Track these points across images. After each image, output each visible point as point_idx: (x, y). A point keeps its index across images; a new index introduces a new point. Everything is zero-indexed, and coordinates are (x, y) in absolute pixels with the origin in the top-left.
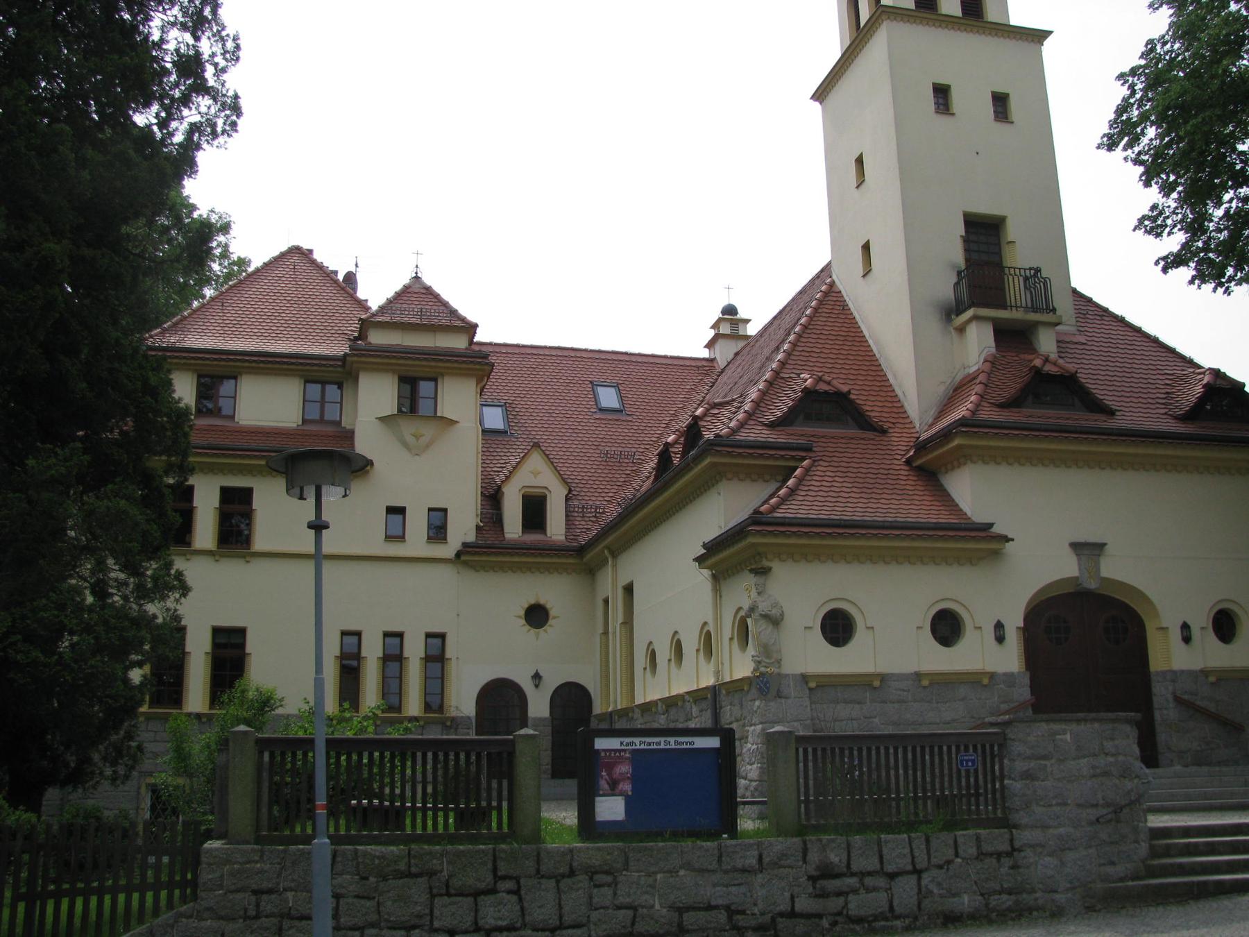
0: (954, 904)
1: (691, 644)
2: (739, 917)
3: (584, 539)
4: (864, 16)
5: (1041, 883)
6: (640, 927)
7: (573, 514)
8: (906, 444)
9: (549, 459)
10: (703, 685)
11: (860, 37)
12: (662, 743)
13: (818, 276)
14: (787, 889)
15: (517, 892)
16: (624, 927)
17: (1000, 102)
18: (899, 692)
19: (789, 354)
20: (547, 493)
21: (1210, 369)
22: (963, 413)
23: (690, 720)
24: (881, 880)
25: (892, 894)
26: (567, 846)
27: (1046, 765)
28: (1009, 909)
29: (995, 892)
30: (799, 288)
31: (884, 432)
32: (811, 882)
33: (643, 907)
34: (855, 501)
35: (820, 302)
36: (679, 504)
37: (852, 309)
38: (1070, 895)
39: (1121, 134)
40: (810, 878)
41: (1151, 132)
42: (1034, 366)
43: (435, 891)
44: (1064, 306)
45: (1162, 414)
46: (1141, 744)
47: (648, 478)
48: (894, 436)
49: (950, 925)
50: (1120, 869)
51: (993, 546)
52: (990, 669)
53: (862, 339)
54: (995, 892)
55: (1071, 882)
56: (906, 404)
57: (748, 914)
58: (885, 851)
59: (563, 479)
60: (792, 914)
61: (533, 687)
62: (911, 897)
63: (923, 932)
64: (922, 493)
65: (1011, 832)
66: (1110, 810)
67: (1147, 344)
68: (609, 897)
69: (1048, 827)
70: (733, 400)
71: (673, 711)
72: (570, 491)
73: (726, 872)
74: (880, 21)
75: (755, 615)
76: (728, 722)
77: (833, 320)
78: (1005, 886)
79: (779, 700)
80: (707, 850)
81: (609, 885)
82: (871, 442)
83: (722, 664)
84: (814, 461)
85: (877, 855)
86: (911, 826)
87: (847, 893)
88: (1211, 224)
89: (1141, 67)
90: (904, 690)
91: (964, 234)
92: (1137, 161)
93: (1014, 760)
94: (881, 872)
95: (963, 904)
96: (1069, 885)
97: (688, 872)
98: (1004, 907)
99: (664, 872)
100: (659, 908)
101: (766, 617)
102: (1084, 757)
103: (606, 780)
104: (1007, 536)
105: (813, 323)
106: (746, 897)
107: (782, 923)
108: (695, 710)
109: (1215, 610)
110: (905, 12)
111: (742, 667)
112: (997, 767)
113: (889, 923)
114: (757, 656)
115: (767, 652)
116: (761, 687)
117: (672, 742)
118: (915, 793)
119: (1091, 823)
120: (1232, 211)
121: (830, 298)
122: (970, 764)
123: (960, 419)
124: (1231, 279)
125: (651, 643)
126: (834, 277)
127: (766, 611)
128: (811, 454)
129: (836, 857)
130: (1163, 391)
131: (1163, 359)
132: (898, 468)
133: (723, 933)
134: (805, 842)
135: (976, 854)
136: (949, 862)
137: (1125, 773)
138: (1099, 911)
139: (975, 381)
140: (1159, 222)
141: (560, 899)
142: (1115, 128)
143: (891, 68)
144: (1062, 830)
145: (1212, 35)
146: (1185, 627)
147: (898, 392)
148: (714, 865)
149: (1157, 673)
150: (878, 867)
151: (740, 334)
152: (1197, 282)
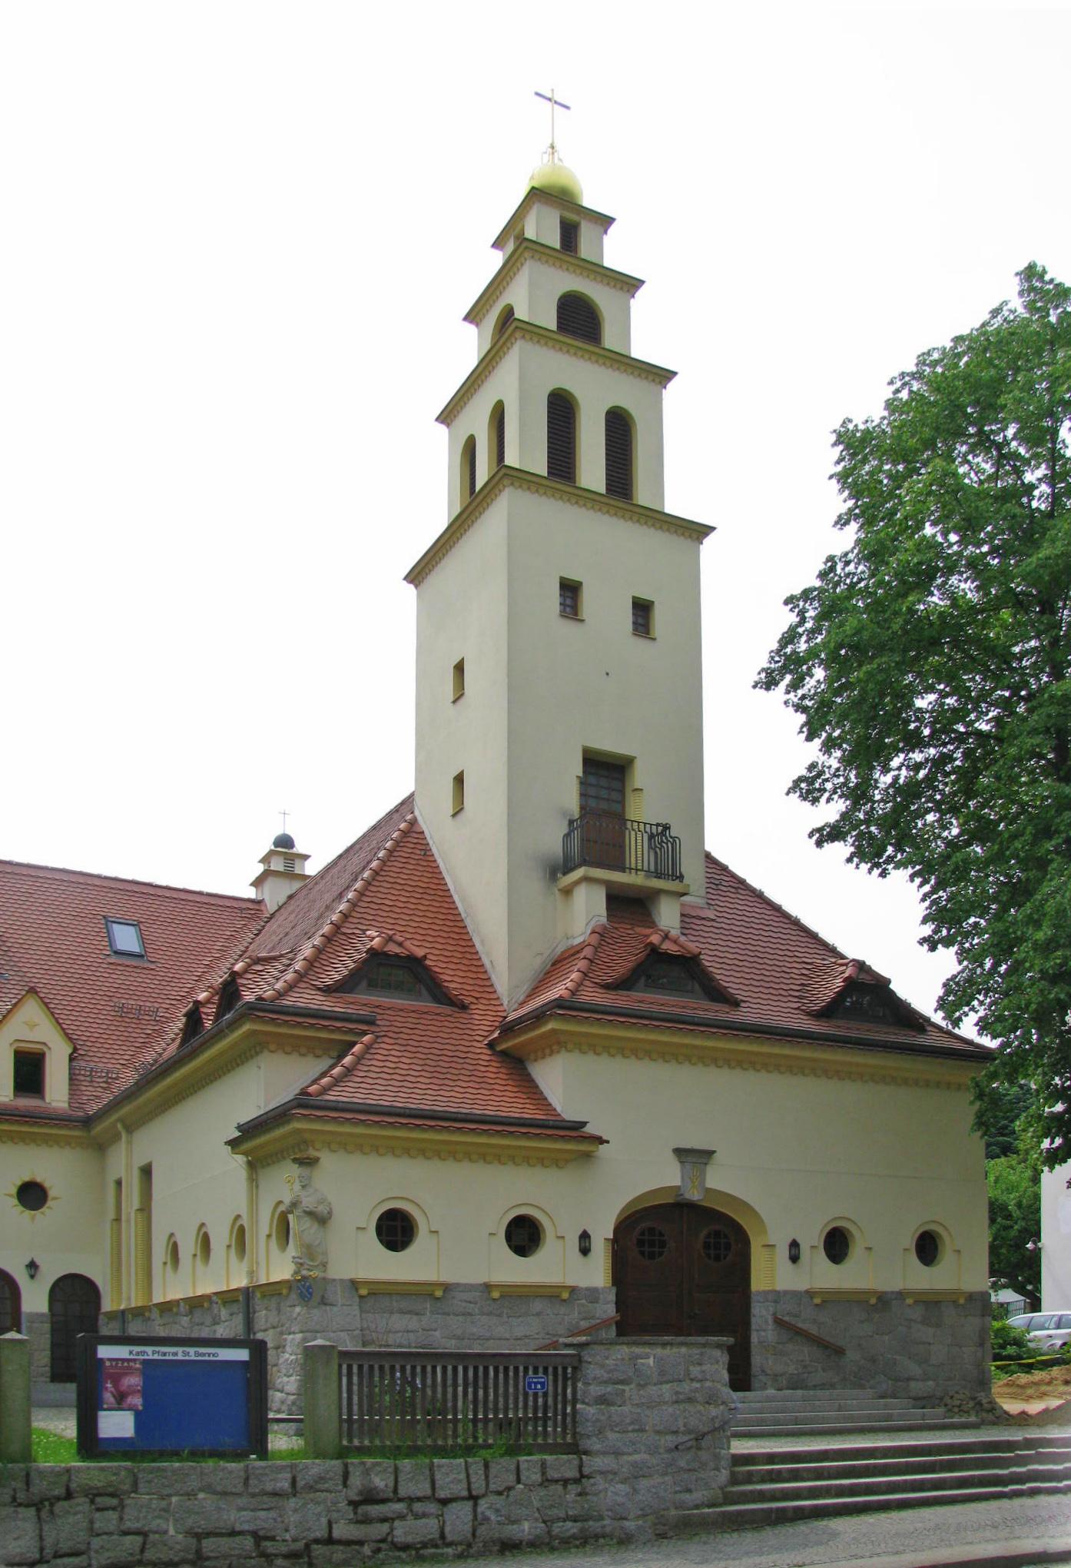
0: (512, 1531)
1: (220, 1238)
2: (268, 1544)
3: (93, 1108)
4: (482, 478)
5: (611, 1510)
6: (150, 1555)
7: (78, 1077)
8: (490, 1023)
9: (48, 1008)
10: (234, 1286)
11: (475, 504)
13: (397, 810)
14: (324, 1513)
16: (131, 1554)
17: (642, 610)
18: (464, 1304)
19: (354, 904)
20: (45, 1049)
21: (854, 960)
22: (561, 992)
23: (218, 1324)
24: (432, 1505)
25: (444, 1522)
26: (63, 1465)
27: (624, 1391)
28: (574, 1537)
29: (559, 1519)
30: (372, 821)
31: (464, 1007)
32: (351, 1508)
33: (156, 1532)
34: (424, 1086)
35: (397, 843)
36: (240, 1056)
37: (437, 856)
38: (640, 1522)
39: (784, 670)
40: (351, 1503)
41: (819, 673)
42: (651, 943)
44: (693, 873)
45: (795, 1009)
46: (732, 1369)
47: (173, 1040)
48: (478, 1011)
49: (507, 1553)
50: (698, 1496)
51: (584, 1147)
52: (570, 1282)
53: (446, 894)
54: (559, 1519)
55: (642, 1510)
56: (493, 978)
57: (278, 1541)
58: (438, 1476)
59: (67, 1034)
60: (330, 1541)
61: (27, 1277)
62: (466, 1524)
63: (477, 1560)
64: (504, 1083)
65: (581, 1459)
66: (692, 1436)
67: (786, 926)
68: (114, 1522)
69: (623, 1454)
70: (282, 956)
71: (198, 1313)
72: (75, 1050)
73: (253, 1495)
74: (501, 487)
75: (298, 1212)
76: (262, 1328)
77: (411, 867)
78: (570, 1513)
79: (324, 1307)
80: (231, 1472)
81: (114, 1509)
82: (449, 1019)
83: (258, 1263)
84: (377, 1037)
85: (429, 1480)
86: (468, 1451)
87: (393, 1519)
88: (876, 792)
89: (815, 589)
90: (470, 1302)
91: (581, 774)
92: (799, 708)
93: (589, 1384)
94: (433, 1498)
95: (523, 1531)
96: (640, 1513)
97: (208, 1496)
98: (568, 1534)
99: (182, 1495)
100: (174, 1534)
101: (310, 1214)
102: (667, 1382)
103: (112, 1392)
104: (601, 1138)
105: (386, 868)
106: (276, 1522)
107: (318, 1550)
108: (224, 1313)
109: (834, 1225)
110: (529, 478)
111: (280, 1268)
112: (569, 1391)
113: (439, 1551)
114: (298, 1257)
115: (310, 1253)
116: (302, 1292)
117: (192, 1353)
118: (475, 1414)
119: (669, 1451)
120: (901, 781)
121: (409, 839)
122: (539, 1386)
123: (556, 999)
124: (890, 860)
125: (172, 1235)
126: (417, 813)
127: (311, 1208)
128: (373, 1028)
129: (381, 1482)
130: (798, 982)
131: (802, 945)
132: (479, 1051)
133: (248, 1560)
134: (346, 1466)
135: (540, 1480)
136: (509, 1489)
137: (711, 1399)
138: (671, 1538)
139: (577, 956)
140: (817, 786)
141: (41, 1530)
142: (778, 662)
143: (509, 552)
144: (637, 1457)
145: (902, 561)
146: (794, 1245)
147: (486, 961)
148: (240, 1488)
149: (759, 1293)
150: (429, 1492)
151: (296, 872)
152: (856, 860)
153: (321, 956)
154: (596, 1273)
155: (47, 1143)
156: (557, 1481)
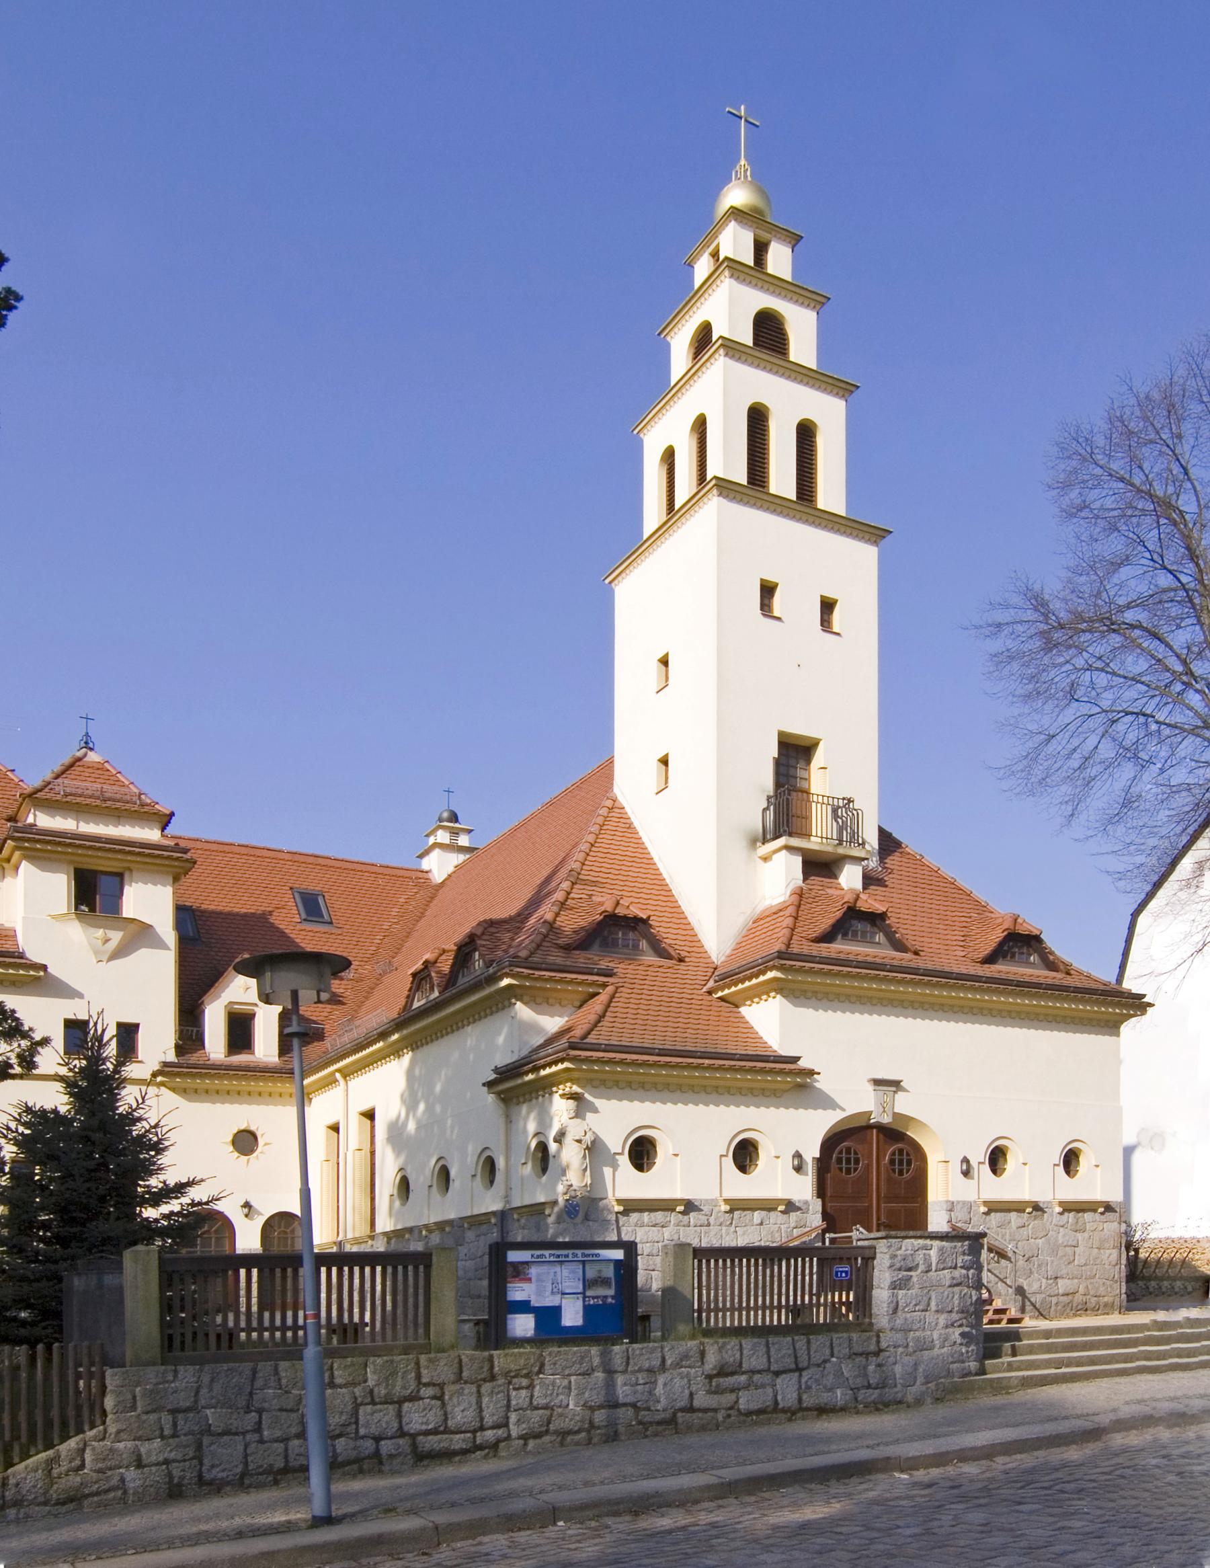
12: (571, 1256)
15: (440, 1398)
33: (560, 1407)
43: (359, 1400)
122: (844, 1275)
154: (803, 1188)
156: (861, 1354)
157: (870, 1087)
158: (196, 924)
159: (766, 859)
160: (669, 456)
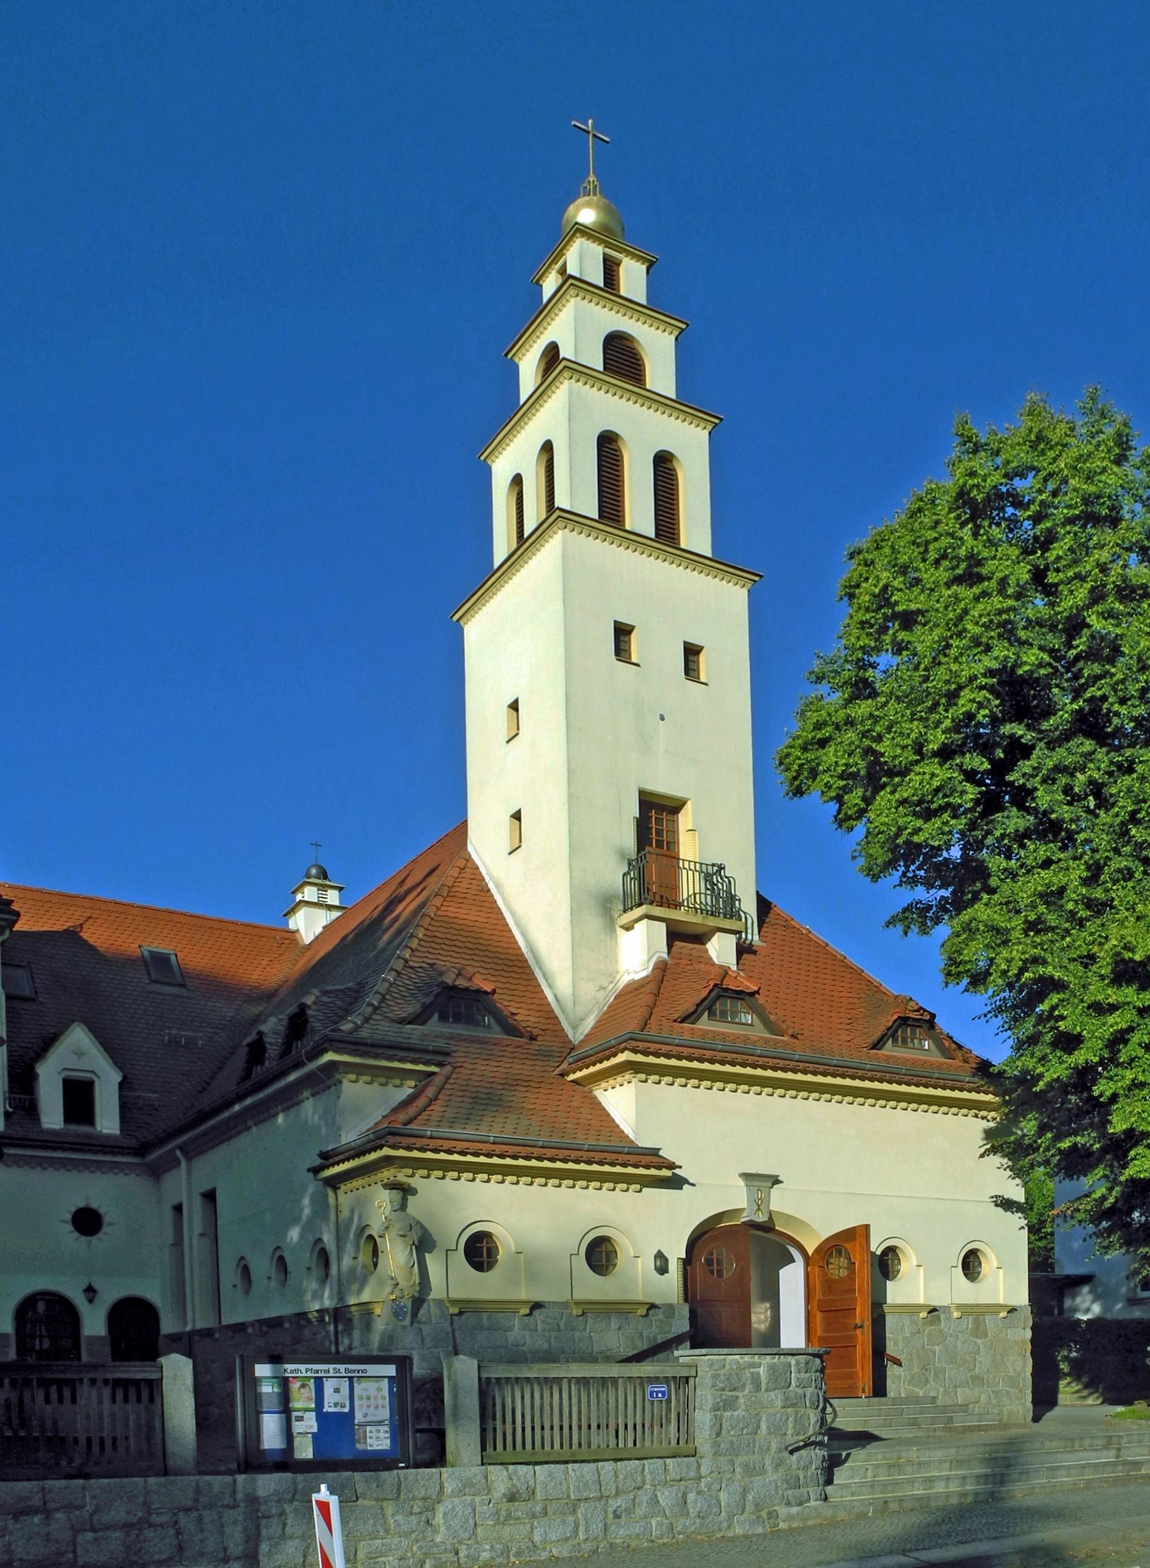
12: (331, 1371)
27: (737, 1397)
84: (455, 1068)
91: (638, 816)
122: (660, 1395)
153: (392, 989)
155: (64, 1167)
157: (741, 1183)
158: (33, 982)
159: (628, 928)
160: (517, 480)
